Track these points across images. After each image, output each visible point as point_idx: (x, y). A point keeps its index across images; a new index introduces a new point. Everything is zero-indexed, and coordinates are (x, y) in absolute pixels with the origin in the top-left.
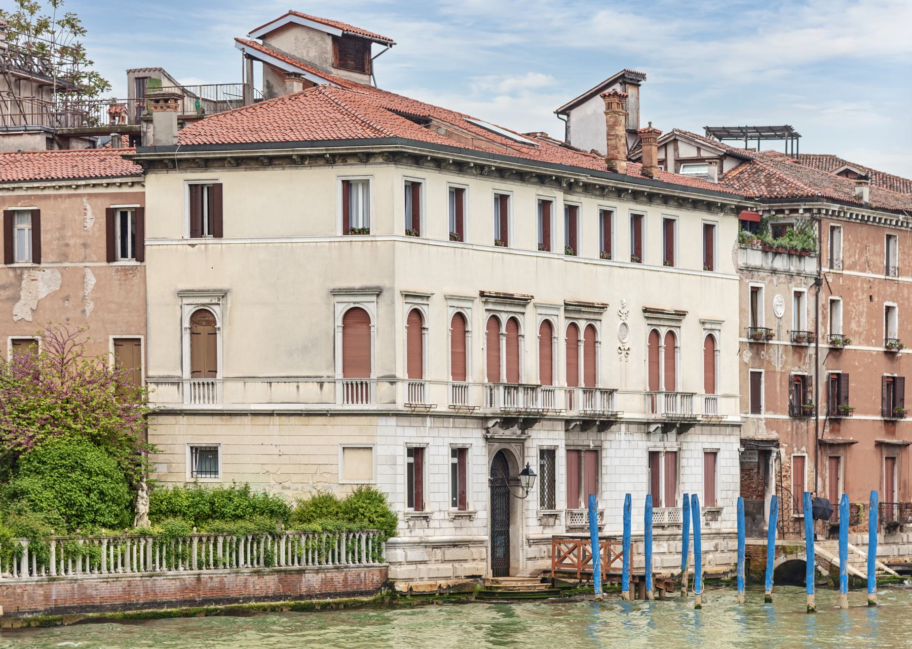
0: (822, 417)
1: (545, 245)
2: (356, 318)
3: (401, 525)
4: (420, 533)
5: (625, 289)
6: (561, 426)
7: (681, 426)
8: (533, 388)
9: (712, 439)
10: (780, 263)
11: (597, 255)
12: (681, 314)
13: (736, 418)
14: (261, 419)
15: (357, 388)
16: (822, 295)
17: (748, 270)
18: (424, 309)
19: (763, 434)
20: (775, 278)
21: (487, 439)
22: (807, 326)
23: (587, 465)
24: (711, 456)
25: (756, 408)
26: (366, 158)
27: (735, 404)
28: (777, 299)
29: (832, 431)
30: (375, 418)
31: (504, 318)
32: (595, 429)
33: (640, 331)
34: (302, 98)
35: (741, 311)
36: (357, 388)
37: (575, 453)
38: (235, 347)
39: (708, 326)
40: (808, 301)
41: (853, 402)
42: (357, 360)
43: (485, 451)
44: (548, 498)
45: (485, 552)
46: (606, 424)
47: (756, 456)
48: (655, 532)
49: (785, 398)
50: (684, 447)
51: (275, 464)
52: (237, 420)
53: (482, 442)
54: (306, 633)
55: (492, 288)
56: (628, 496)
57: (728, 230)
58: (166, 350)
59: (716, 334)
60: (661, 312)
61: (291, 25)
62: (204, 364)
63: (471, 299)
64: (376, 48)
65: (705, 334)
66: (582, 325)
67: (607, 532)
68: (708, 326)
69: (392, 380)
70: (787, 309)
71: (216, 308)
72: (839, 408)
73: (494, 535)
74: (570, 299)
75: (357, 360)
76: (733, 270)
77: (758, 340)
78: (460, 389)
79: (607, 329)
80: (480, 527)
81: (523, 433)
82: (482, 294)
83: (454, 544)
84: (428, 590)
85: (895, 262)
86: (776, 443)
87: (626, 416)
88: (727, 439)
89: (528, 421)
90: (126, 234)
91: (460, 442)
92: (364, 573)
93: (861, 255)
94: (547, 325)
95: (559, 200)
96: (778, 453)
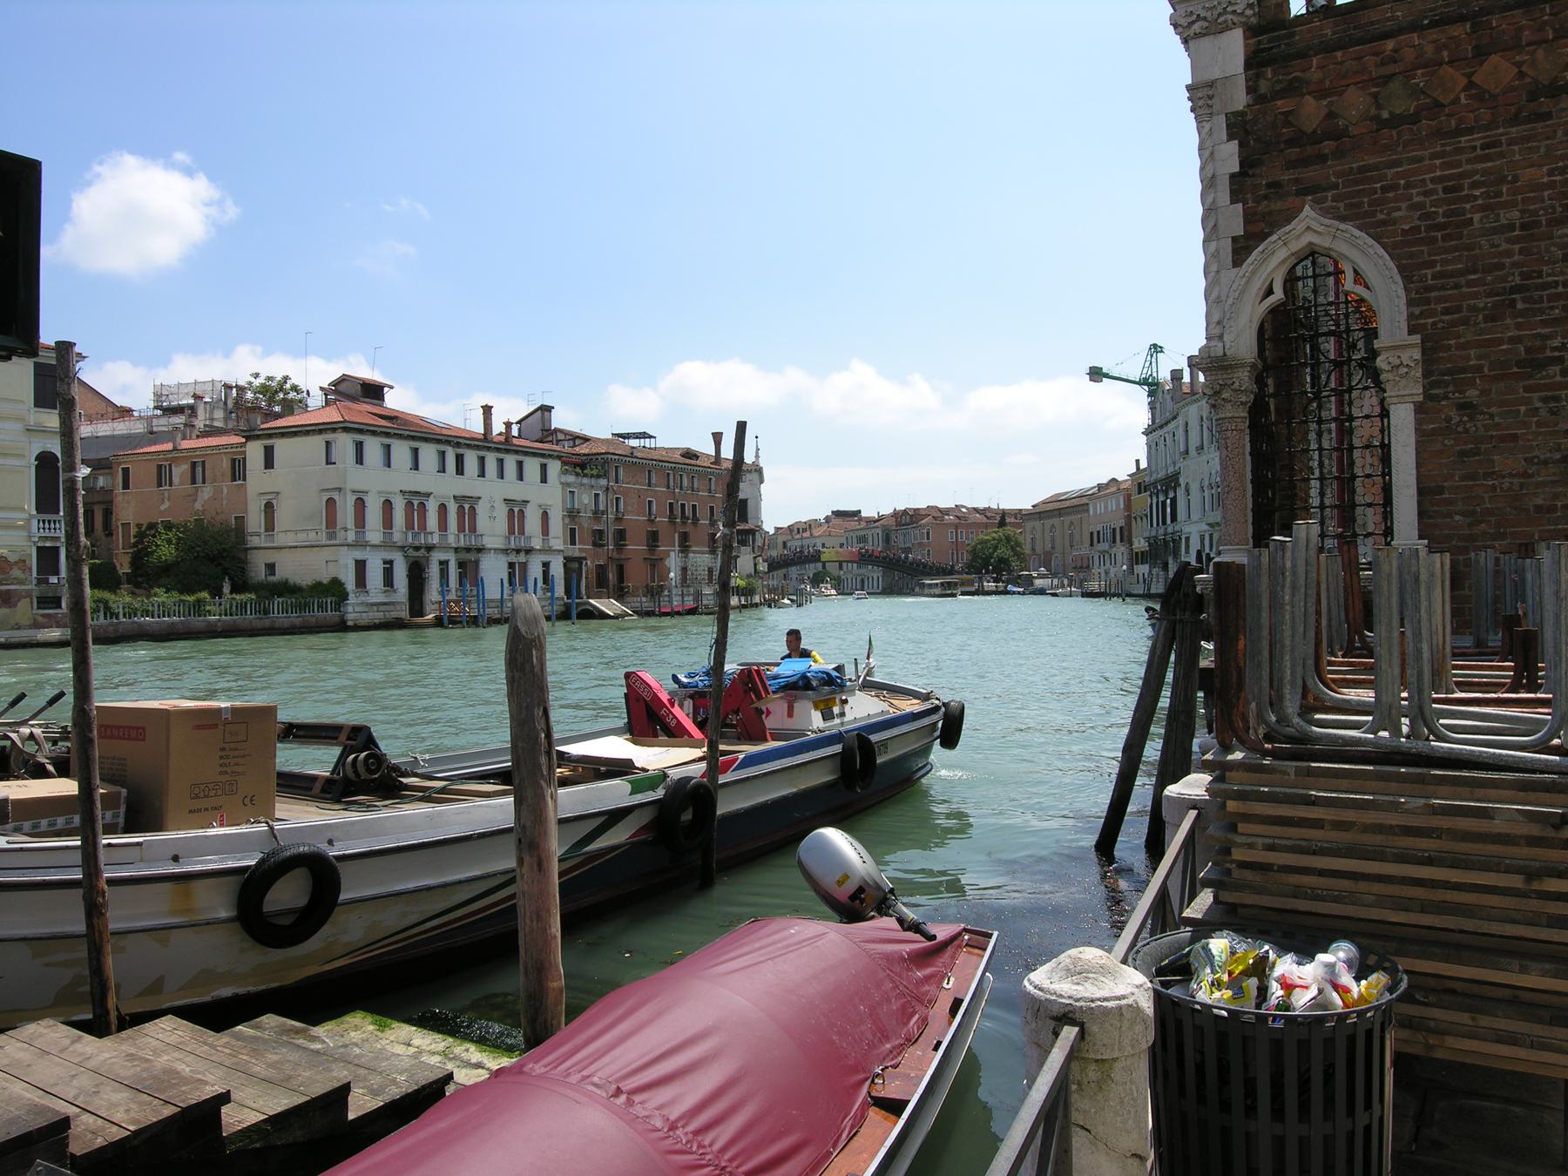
1: (443, 470)
2: (331, 502)
3: (351, 596)
4: (363, 598)
10: (585, 481)
15: (332, 536)
19: (577, 554)
24: (546, 565)
25: (573, 542)
26: (334, 430)
31: (416, 503)
33: (502, 512)
36: (332, 536)
37: (461, 565)
38: (282, 518)
42: (331, 521)
46: (480, 550)
51: (299, 568)
57: (554, 467)
58: (255, 521)
62: (270, 526)
66: (467, 506)
69: (346, 530)
75: (331, 521)
79: (482, 510)
85: (653, 481)
90: (238, 469)
92: (331, 615)
94: (443, 508)
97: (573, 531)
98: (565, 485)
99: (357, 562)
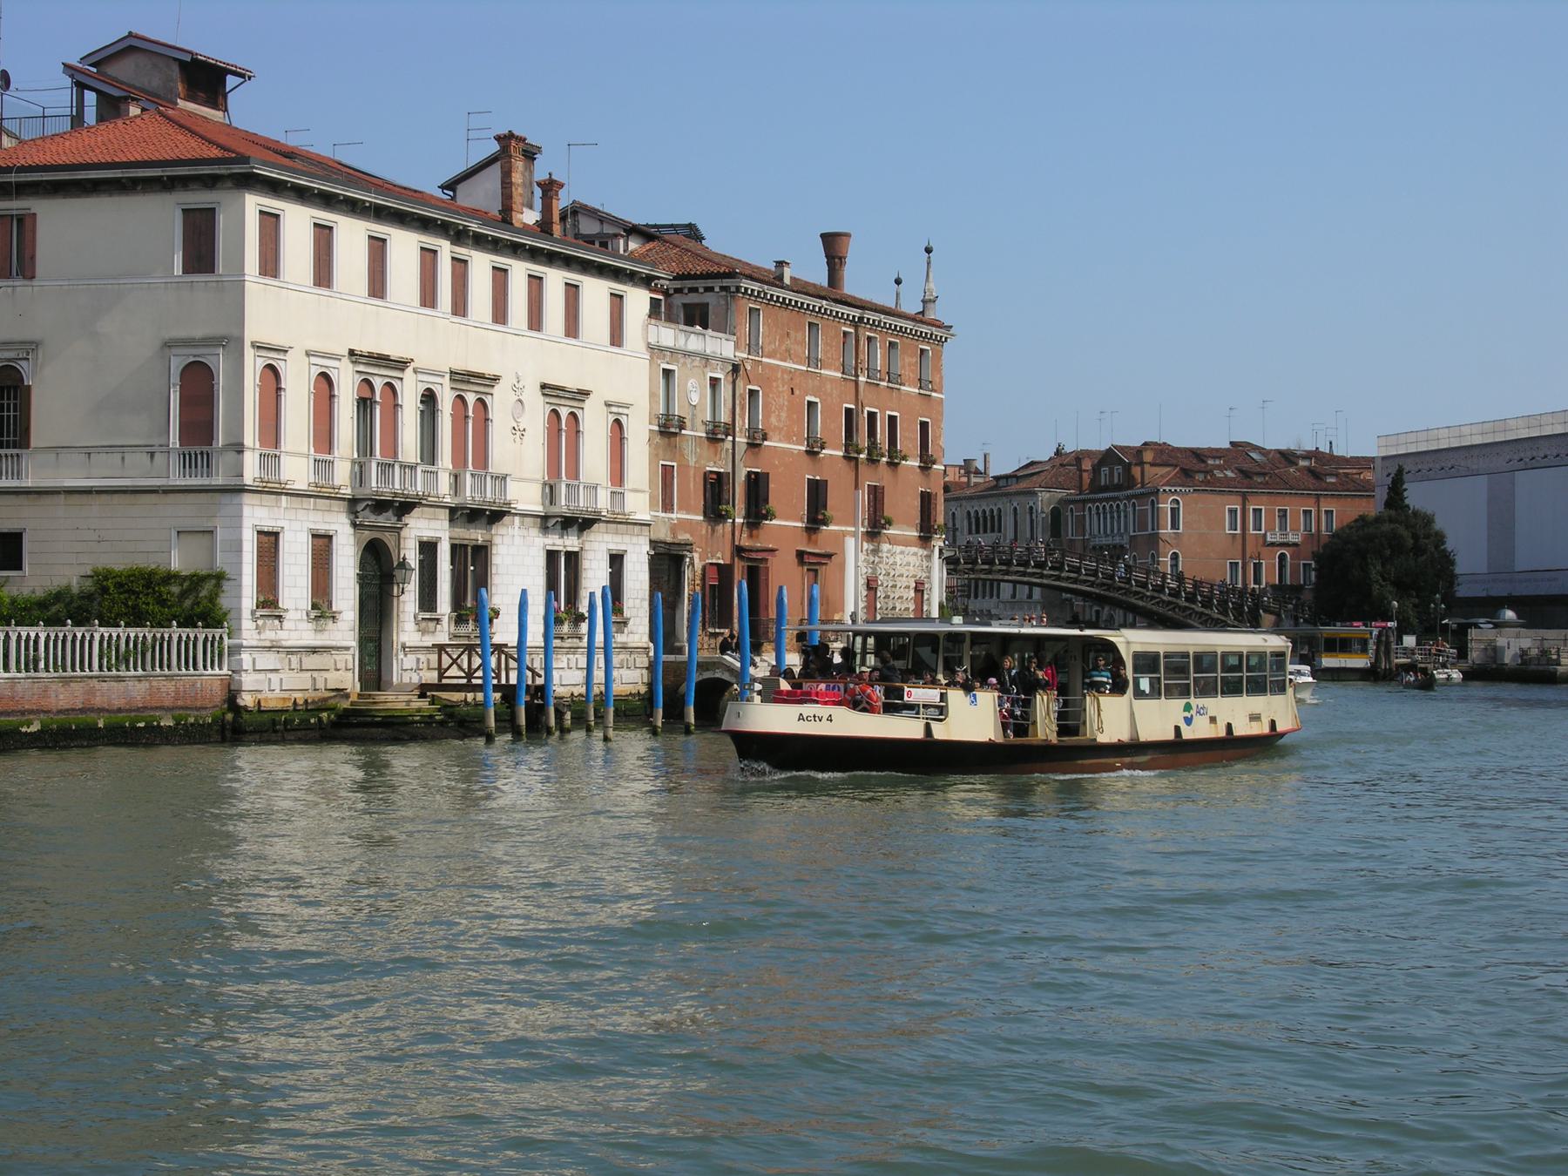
0: (739, 520)
5: (522, 360)
6: (445, 514)
7: (581, 523)
8: (413, 468)
9: (618, 538)
11: (489, 318)
12: (585, 393)
13: (644, 516)
14: (76, 499)
16: (740, 383)
17: (656, 350)
18: (280, 366)
20: (689, 360)
21: (354, 525)
22: (724, 417)
23: (474, 564)
24: (616, 560)
25: (667, 506)
27: (644, 499)
28: (692, 382)
29: (751, 536)
30: (217, 495)
32: (484, 520)
33: (537, 412)
34: (138, 121)
35: (653, 395)
39: (614, 409)
40: (725, 391)
41: (774, 503)
43: (352, 540)
44: (428, 600)
45: (351, 659)
46: (495, 516)
47: (667, 562)
48: (556, 643)
49: (697, 497)
50: (587, 547)
52: (47, 500)
53: (350, 530)
54: (297, 1125)
55: (364, 347)
56: (524, 592)
57: (638, 300)
59: (623, 420)
60: (562, 389)
61: (131, 50)
63: (337, 358)
64: (231, 81)
65: (611, 418)
67: (497, 640)
68: (614, 409)
70: (702, 396)
71: (23, 363)
72: (758, 510)
73: (363, 641)
74: (460, 366)
76: (642, 348)
77: (668, 429)
78: (323, 466)
79: (500, 401)
80: (345, 630)
81: (399, 520)
82: (352, 353)
83: (314, 650)
84: (279, 706)
86: (688, 546)
87: (521, 506)
88: (635, 539)
89: (404, 507)
91: (322, 527)
93: (781, 342)
94: (429, 398)
95: (445, 248)
96: (692, 559)
97: (667, 471)
98: (656, 350)
99: (464, 315)
